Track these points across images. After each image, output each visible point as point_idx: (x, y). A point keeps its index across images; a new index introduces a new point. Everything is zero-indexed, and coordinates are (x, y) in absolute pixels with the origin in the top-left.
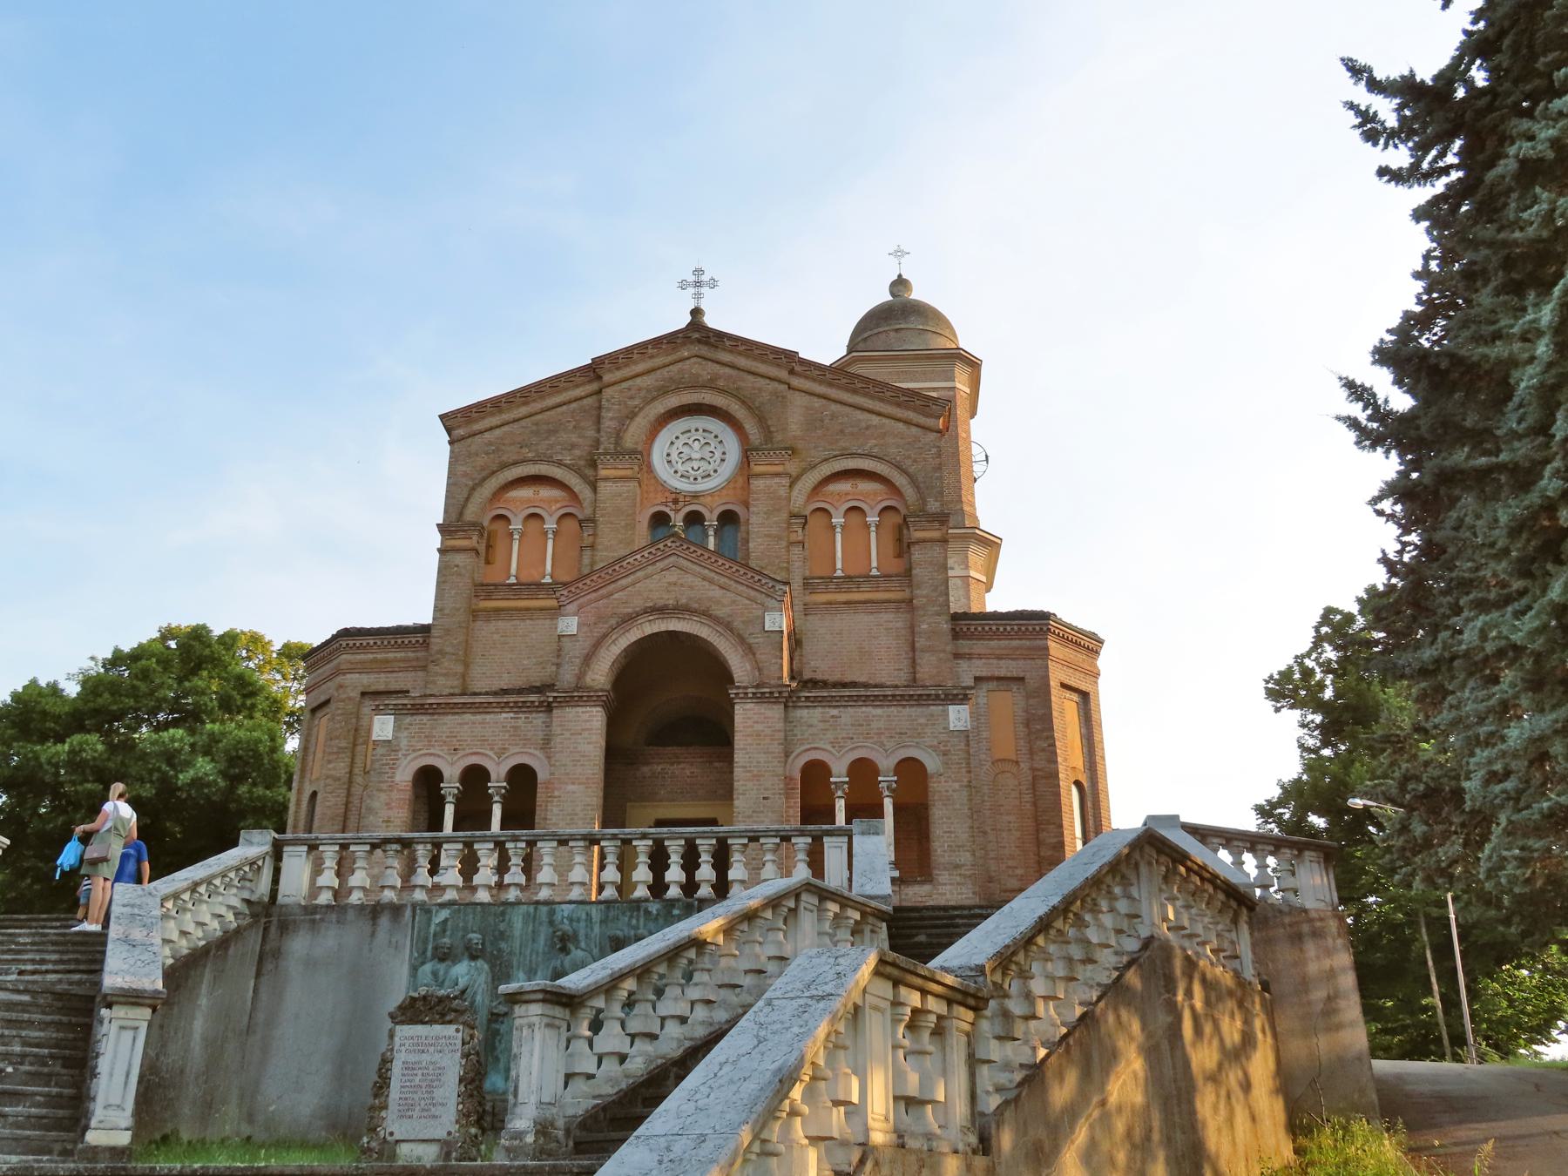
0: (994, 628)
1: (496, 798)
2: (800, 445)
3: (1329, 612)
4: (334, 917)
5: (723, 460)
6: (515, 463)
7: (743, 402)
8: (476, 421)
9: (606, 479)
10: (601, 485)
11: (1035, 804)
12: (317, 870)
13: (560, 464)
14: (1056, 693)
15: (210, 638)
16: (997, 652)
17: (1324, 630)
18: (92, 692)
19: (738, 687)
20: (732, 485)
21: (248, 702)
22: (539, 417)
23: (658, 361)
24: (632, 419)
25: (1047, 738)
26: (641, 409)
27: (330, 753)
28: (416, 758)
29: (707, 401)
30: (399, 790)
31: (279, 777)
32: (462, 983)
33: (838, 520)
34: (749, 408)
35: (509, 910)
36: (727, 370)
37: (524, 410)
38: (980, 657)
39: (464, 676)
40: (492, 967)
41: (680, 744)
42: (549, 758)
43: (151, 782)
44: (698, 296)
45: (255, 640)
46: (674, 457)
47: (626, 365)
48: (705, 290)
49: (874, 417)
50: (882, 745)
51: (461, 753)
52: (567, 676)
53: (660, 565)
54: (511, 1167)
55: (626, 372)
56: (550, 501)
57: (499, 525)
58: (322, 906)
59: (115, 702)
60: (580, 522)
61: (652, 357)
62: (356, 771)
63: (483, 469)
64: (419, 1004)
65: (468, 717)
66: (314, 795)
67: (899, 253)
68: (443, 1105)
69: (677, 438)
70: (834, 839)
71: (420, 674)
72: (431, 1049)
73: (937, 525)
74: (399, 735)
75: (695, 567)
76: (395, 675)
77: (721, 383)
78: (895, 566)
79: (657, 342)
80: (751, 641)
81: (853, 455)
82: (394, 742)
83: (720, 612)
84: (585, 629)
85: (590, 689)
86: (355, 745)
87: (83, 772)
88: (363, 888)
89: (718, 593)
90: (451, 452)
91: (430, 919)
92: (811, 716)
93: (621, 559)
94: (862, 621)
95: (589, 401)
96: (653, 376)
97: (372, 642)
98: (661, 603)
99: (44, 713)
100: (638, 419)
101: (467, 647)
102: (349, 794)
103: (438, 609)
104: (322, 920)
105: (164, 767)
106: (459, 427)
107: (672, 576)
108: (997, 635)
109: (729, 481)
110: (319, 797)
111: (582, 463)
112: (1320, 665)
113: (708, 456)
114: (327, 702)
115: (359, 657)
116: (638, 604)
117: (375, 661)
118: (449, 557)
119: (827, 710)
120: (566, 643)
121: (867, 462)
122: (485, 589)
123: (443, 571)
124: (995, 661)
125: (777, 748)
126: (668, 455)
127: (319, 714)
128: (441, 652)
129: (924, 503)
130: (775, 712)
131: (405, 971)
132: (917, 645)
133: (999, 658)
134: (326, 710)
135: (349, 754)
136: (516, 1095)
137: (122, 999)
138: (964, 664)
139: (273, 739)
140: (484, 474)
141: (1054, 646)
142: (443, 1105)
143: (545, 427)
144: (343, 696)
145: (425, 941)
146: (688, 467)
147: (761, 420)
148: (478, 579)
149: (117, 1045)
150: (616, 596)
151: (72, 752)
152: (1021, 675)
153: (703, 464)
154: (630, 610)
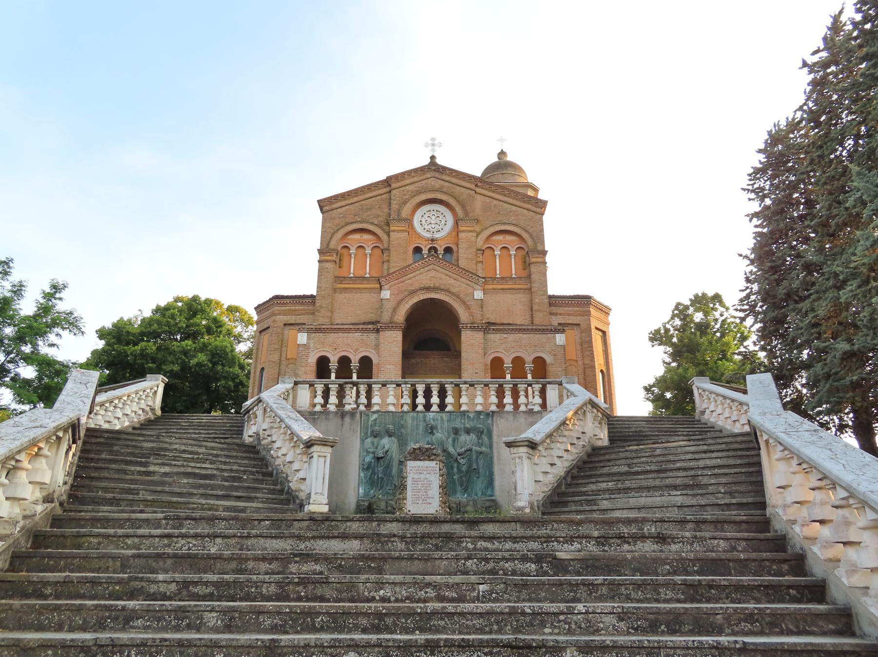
1: (354, 371)
2: (480, 218)
3: (679, 304)
4: (324, 417)
6: (352, 223)
7: (455, 198)
8: (333, 203)
9: (394, 231)
10: (392, 234)
11: (585, 379)
13: (372, 224)
14: (594, 331)
15: (200, 301)
17: (676, 312)
18: (149, 324)
21: (219, 330)
23: (416, 179)
25: (590, 351)
29: (438, 197)
32: (386, 448)
33: (497, 252)
34: (458, 201)
35: (405, 415)
36: (448, 184)
37: (355, 199)
38: (561, 314)
39: (331, 317)
40: (398, 441)
41: (429, 350)
42: (378, 353)
43: (178, 364)
44: (433, 150)
45: (217, 303)
46: (423, 222)
47: (402, 180)
50: (527, 351)
51: (338, 350)
52: (386, 317)
53: (427, 269)
54: (622, 518)
55: (402, 183)
57: (345, 251)
59: (160, 328)
61: (413, 177)
62: (282, 359)
63: (338, 225)
64: (417, 451)
66: (263, 369)
67: (502, 140)
68: (432, 498)
70: (552, 385)
71: (311, 316)
72: (425, 472)
77: (445, 190)
78: (524, 274)
79: (416, 170)
80: (468, 303)
81: (504, 223)
83: (453, 290)
84: (393, 296)
87: (147, 360)
89: (453, 282)
91: (369, 419)
92: (495, 337)
93: (409, 266)
94: (509, 298)
95: (385, 196)
96: (414, 185)
98: (427, 286)
99: (128, 333)
101: (332, 304)
104: (318, 418)
105: (183, 357)
107: (432, 274)
108: (567, 305)
111: (383, 223)
112: (673, 327)
113: (439, 222)
114: (268, 328)
116: (417, 286)
117: (290, 310)
120: (385, 302)
122: (339, 279)
123: (321, 271)
127: (263, 333)
128: (320, 306)
129: (536, 246)
130: (479, 335)
131: (358, 441)
133: (569, 315)
134: (267, 331)
136: (515, 489)
137: (319, 442)
138: (553, 318)
140: (338, 227)
141: (592, 310)
142: (432, 498)
145: (367, 428)
146: (430, 227)
147: (463, 207)
148: (337, 275)
149: (318, 463)
151: (142, 350)
153: (437, 226)
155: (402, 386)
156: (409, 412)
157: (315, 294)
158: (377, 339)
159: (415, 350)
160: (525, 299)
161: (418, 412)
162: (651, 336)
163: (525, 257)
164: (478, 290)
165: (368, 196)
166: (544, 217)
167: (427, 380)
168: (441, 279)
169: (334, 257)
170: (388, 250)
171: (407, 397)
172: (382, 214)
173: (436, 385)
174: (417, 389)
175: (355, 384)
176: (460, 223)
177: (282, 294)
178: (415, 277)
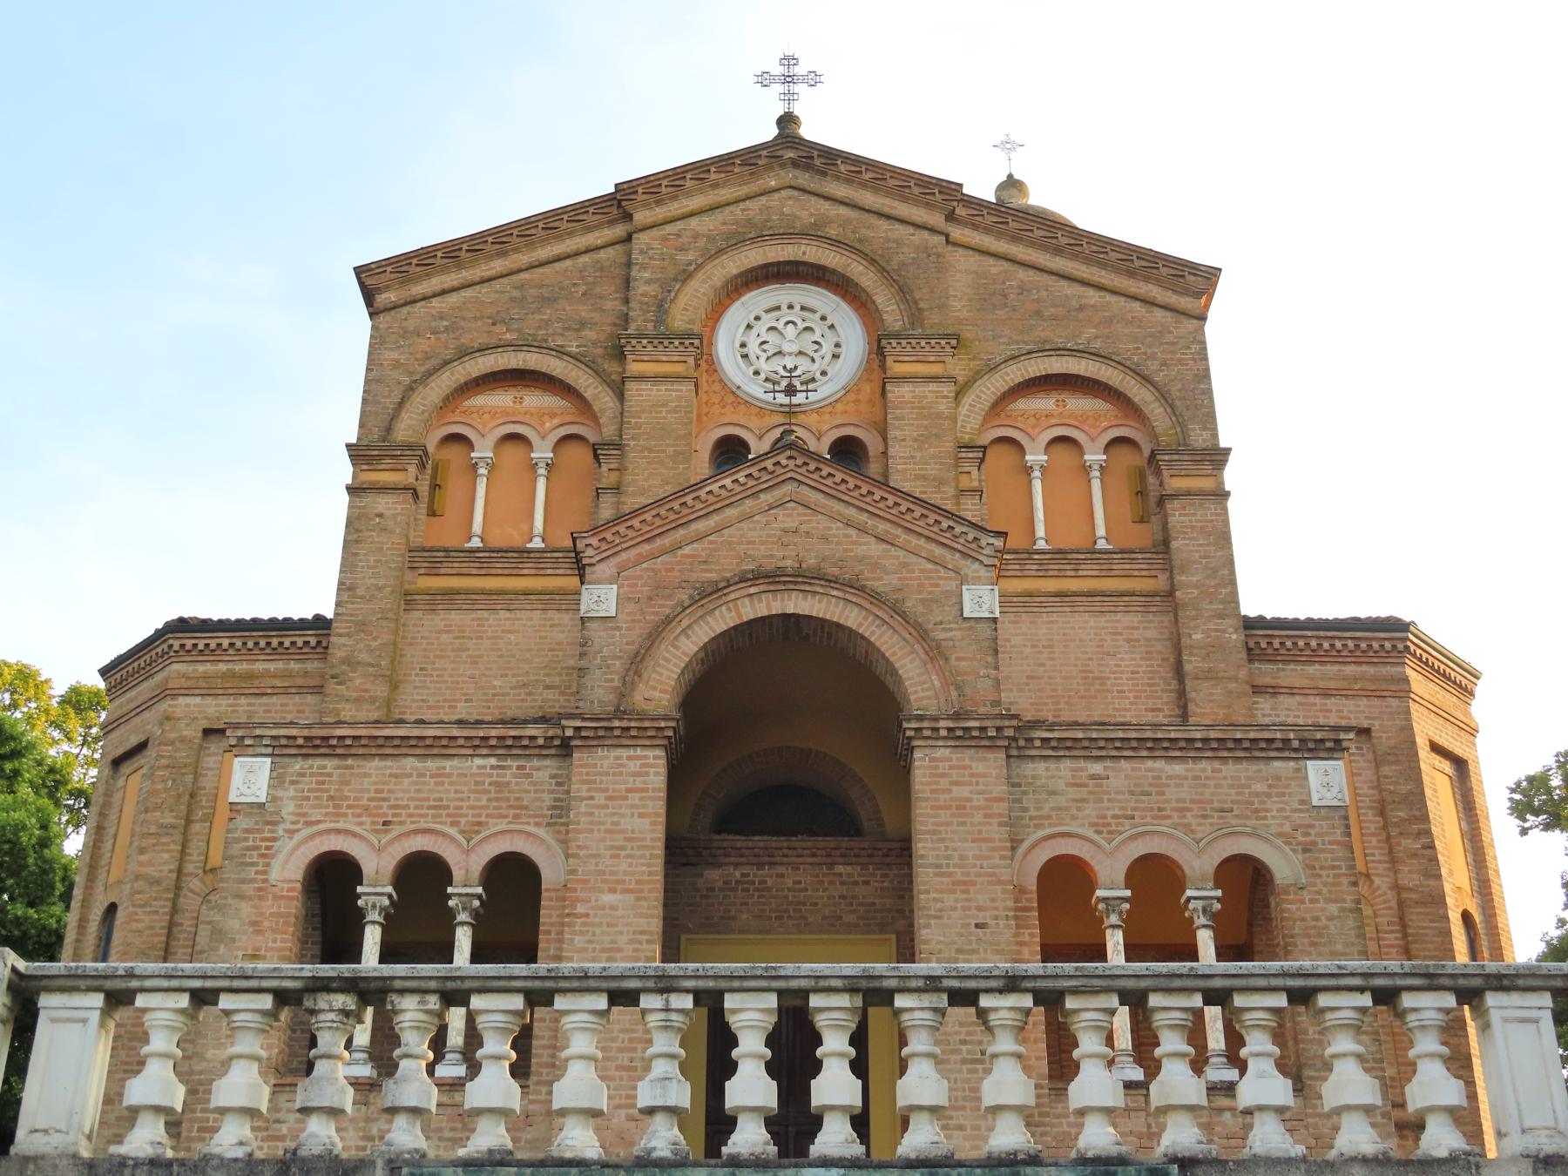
0: (1314, 643)
1: (463, 917)
2: (968, 333)
5: (836, 356)
7: (873, 261)
8: (418, 279)
9: (641, 378)
10: (631, 386)
12: (128, 1062)
13: (560, 352)
14: (1426, 758)
16: (1322, 684)
19: (920, 718)
20: (851, 397)
22: (525, 276)
23: (725, 194)
24: (684, 282)
26: (699, 267)
27: (143, 836)
28: (312, 837)
30: (276, 897)
31: (53, 887)
33: (1035, 457)
36: (843, 211)
37: (498, 265)
42: (564, 842)
44: (789, 97)
46: (753, 348)
47: (675, 198)
48: (799, 88)
49: (1091, 292)
50: (1188, 829)
51: (396, 830)
52: (599, 692)
55: (674, 208)
56: (543, 414)
57: (453, 453)
58: (138, 1163)
60: (595, 449)
61: (715, 186)
62: (189, 868)
63: (427, 358)
65: (410, 763)
66: (112, 909)
67: (1008, 145)
69: (757, 318)
70: (1515, 999)
73: (1208, 467)
74: (280, 793)
75: (831, 503)
76: (264, 700)
77: (833, 232)
78: (1140, 536)
79: (724, 162)
81: (1059, 351)
82: (270, 808)
83: (880, 584)
84: (631, 607)
85: (642, 716)
86: (188, 821)
88: (250, 1112)
89: (874, 549)
90: (373, 327)
94: (1085, 626)
97: (225, 643)
98: (770, 565)
100: (694, 284)
101: (395, 651)
102: (175, 910)
103: (345, 588)
106: (387, 288)
107: (790, 518)
108: (1316, 656)
109: (847, 390)
110: (121, 915)
111: (600, 351)
113: (811, 348)
114: (142, 747)
115: (201, 668)
116: (727, 565)
117: (230, 675)
118: (368, 499)
119: (1082, 763)
120: (596, 632)
121: (1083, 362)
124: (1318, 700)
125: (996, 832)
126: (743, 345)
127: (126, 768)
128: (348, 661)
130: (989, 765)
132: (1188, 667)
133: (1325, 693)
134: (140, 760)
135: (179, 838)
139: (44, 827)
140: (429, 365)
143: (533, 292)
144: (173, 735)
147: (903, 292)
148: (417, 540)
150: (687, 550)
152: (1365, 724)
154: (714, 576)
155: (647, 1001)
156: (681, 1163)
157: (329, 615)
158: (562, 782)
159: (718, 832)
160: (1152, 634)
161: (735, 1162)
162: (1517, 797)
163: (1142, 476)
164: (977, 580)
165: (543, 253)
166: (1210, 328)
167: (788, 968)
168: (825, 539)
169: (409, 475)
170: (619, 446)
171: (672, 1068)
172: (596, 316)
173: (844, 1000)
174: (734, 1021)
175: (372, 993)
176: (892, 347)
177: (203, 615)
178: (718, 530)
